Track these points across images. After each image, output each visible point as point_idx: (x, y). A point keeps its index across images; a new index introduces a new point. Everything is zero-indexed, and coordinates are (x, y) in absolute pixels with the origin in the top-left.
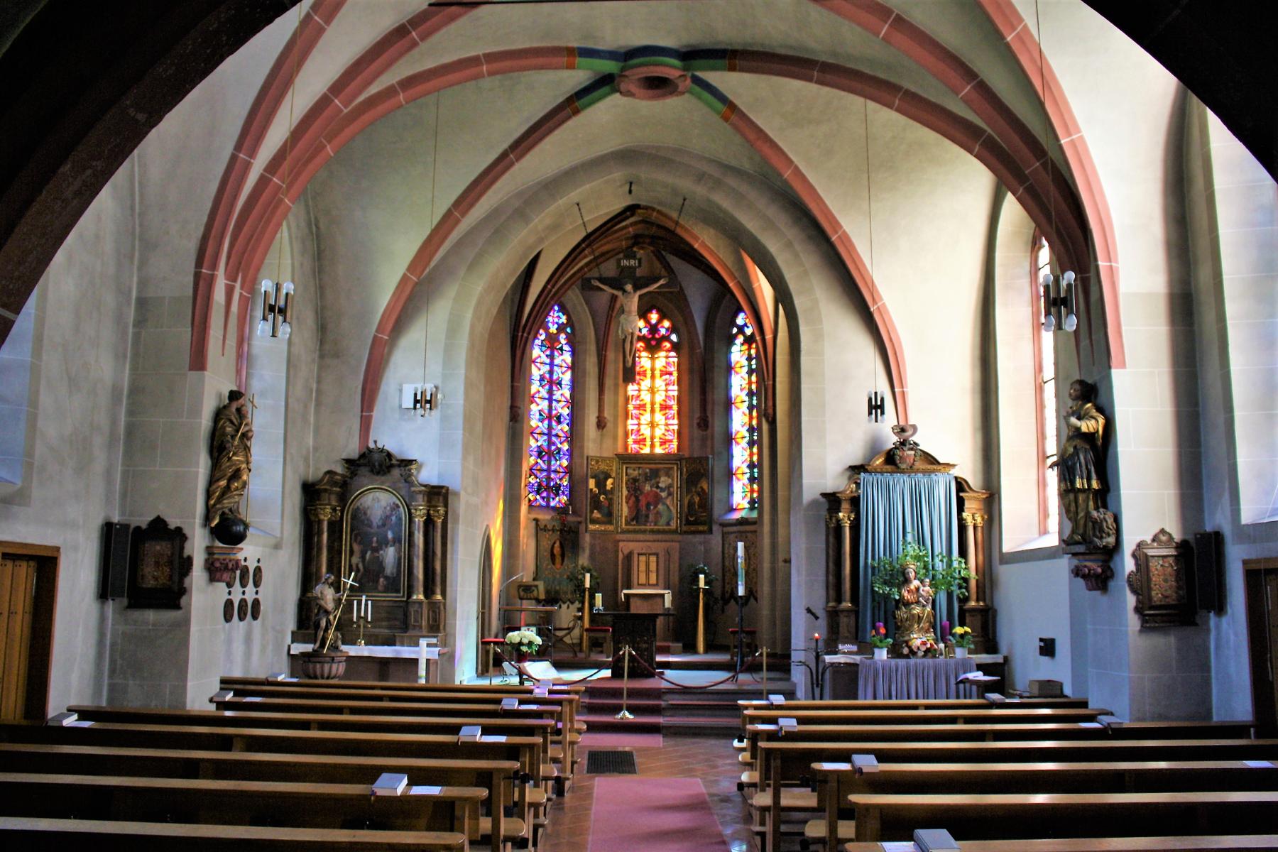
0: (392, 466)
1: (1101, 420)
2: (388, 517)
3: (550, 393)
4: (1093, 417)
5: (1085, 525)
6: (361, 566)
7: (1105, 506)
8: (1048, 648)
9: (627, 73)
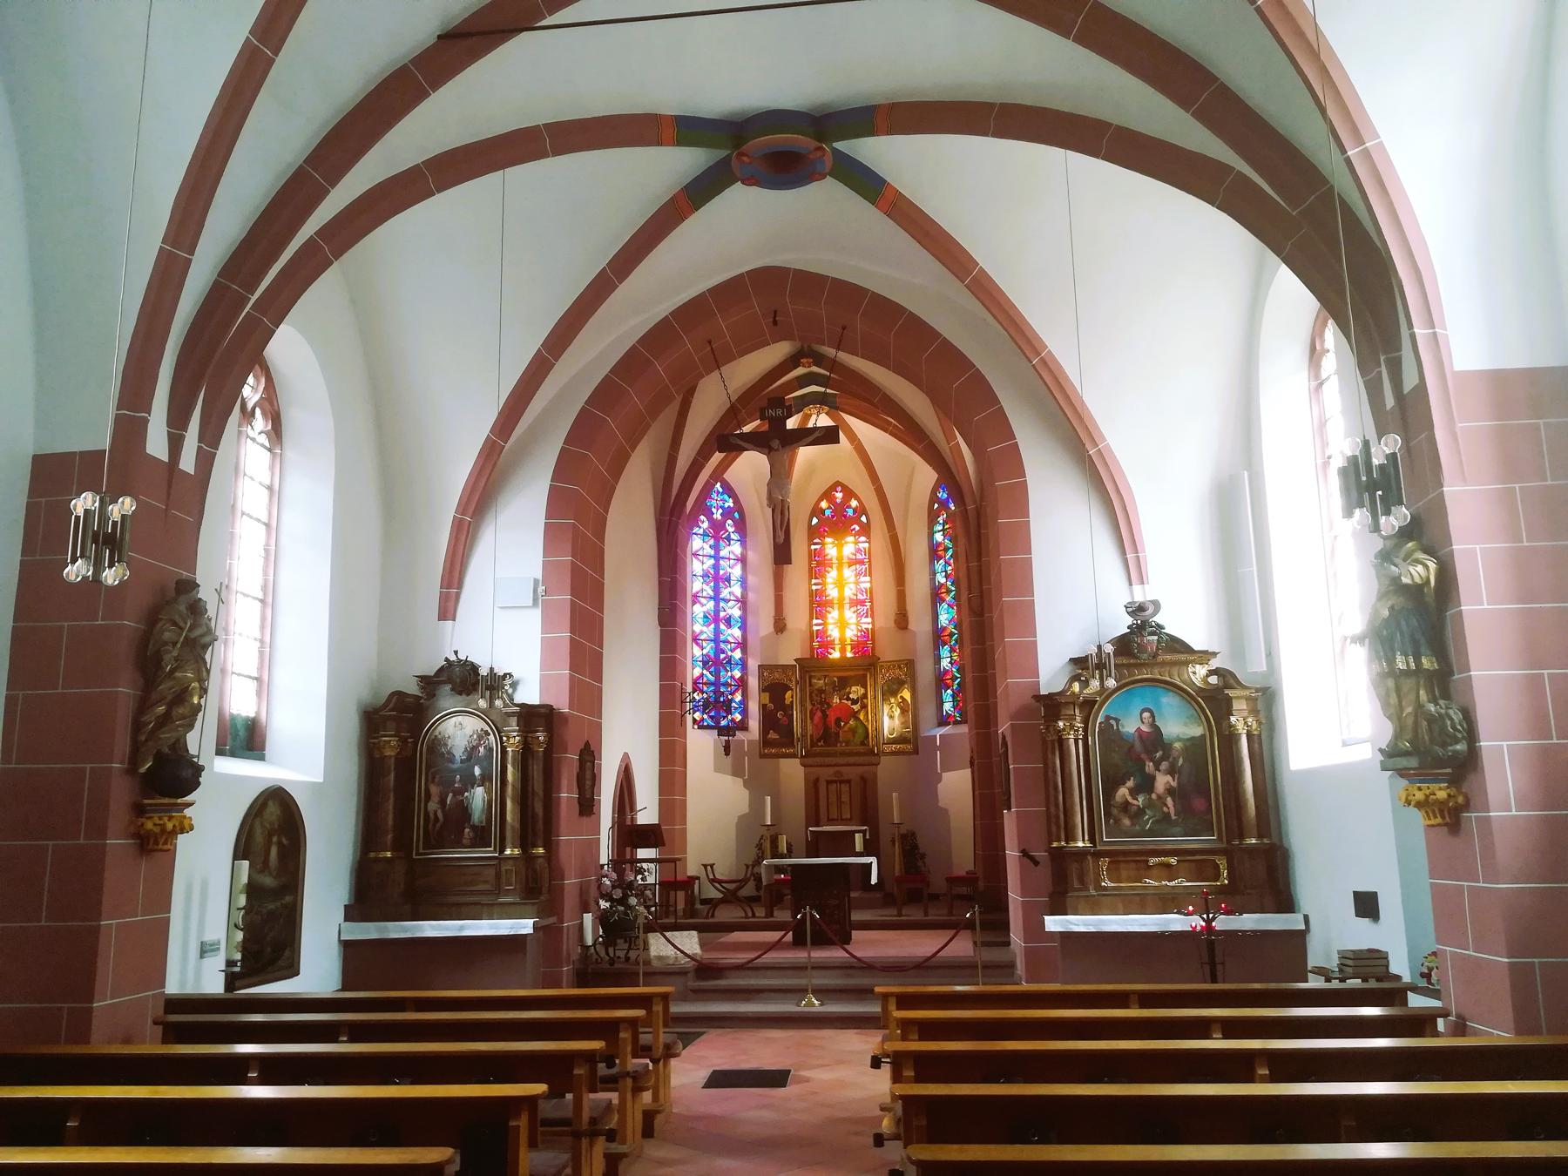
1: (1432, 566)
2: (475, 748)
3: (717, 590)
4: (1418, 561)
5: (1416, 723)
7: (1446, 695)
8: (1367, 905)
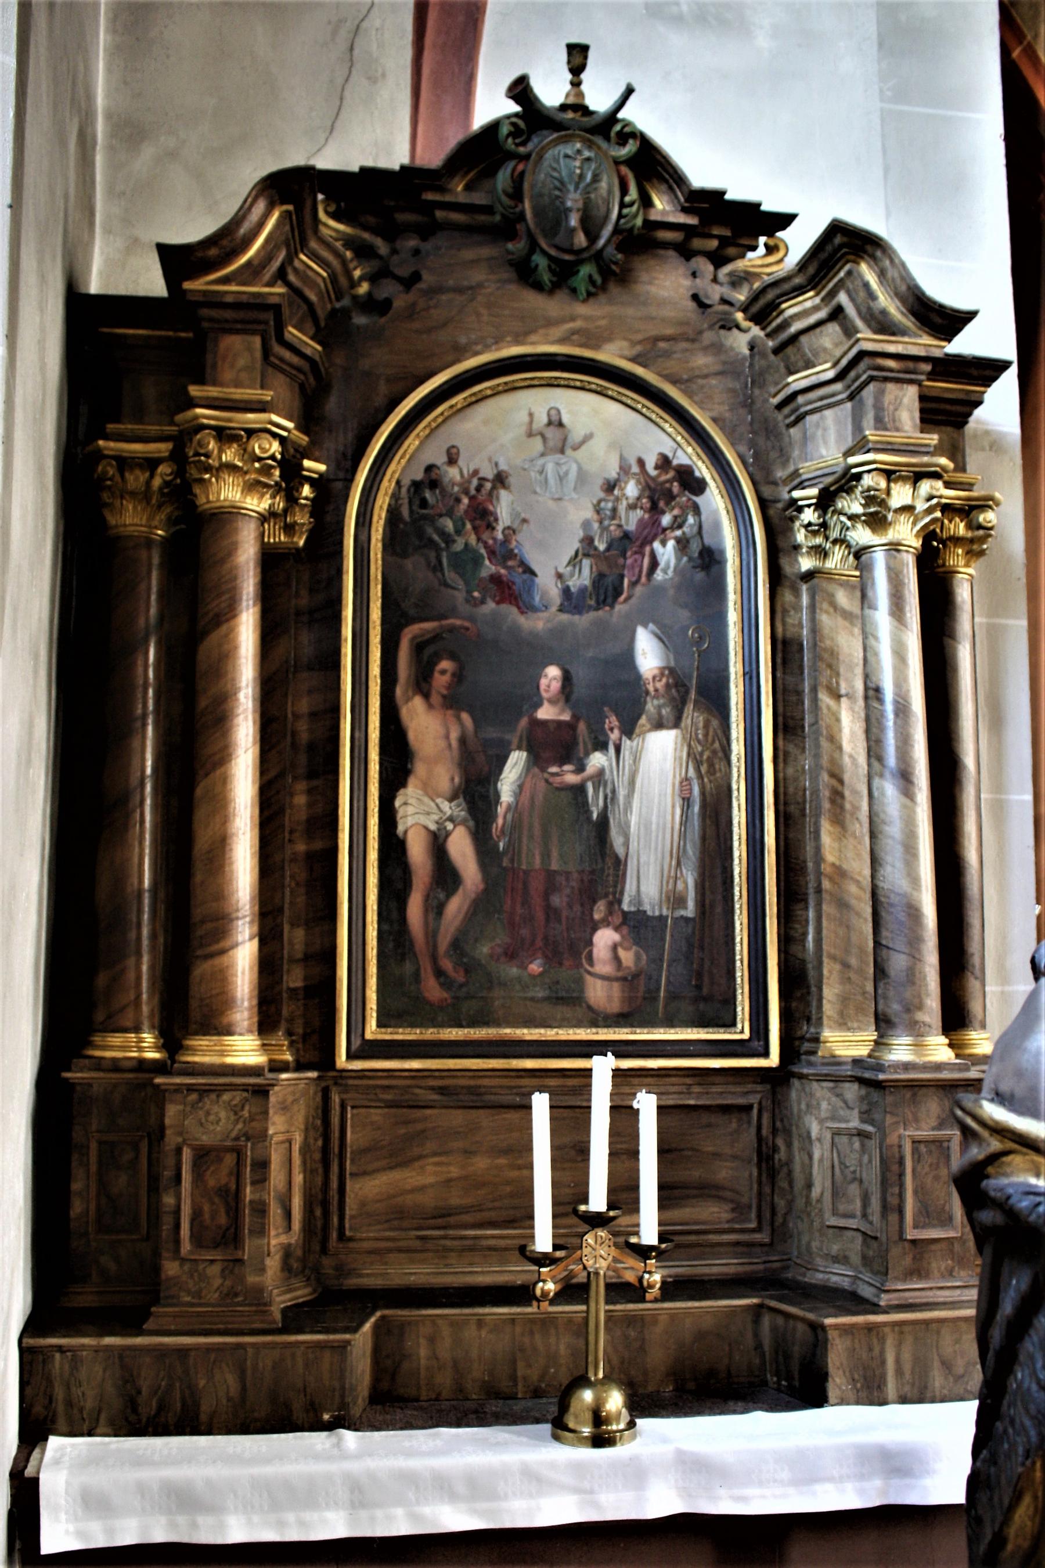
0: (642, 242)
2: (630, 544)
6: (461, 847)
9: (885, 1041)
